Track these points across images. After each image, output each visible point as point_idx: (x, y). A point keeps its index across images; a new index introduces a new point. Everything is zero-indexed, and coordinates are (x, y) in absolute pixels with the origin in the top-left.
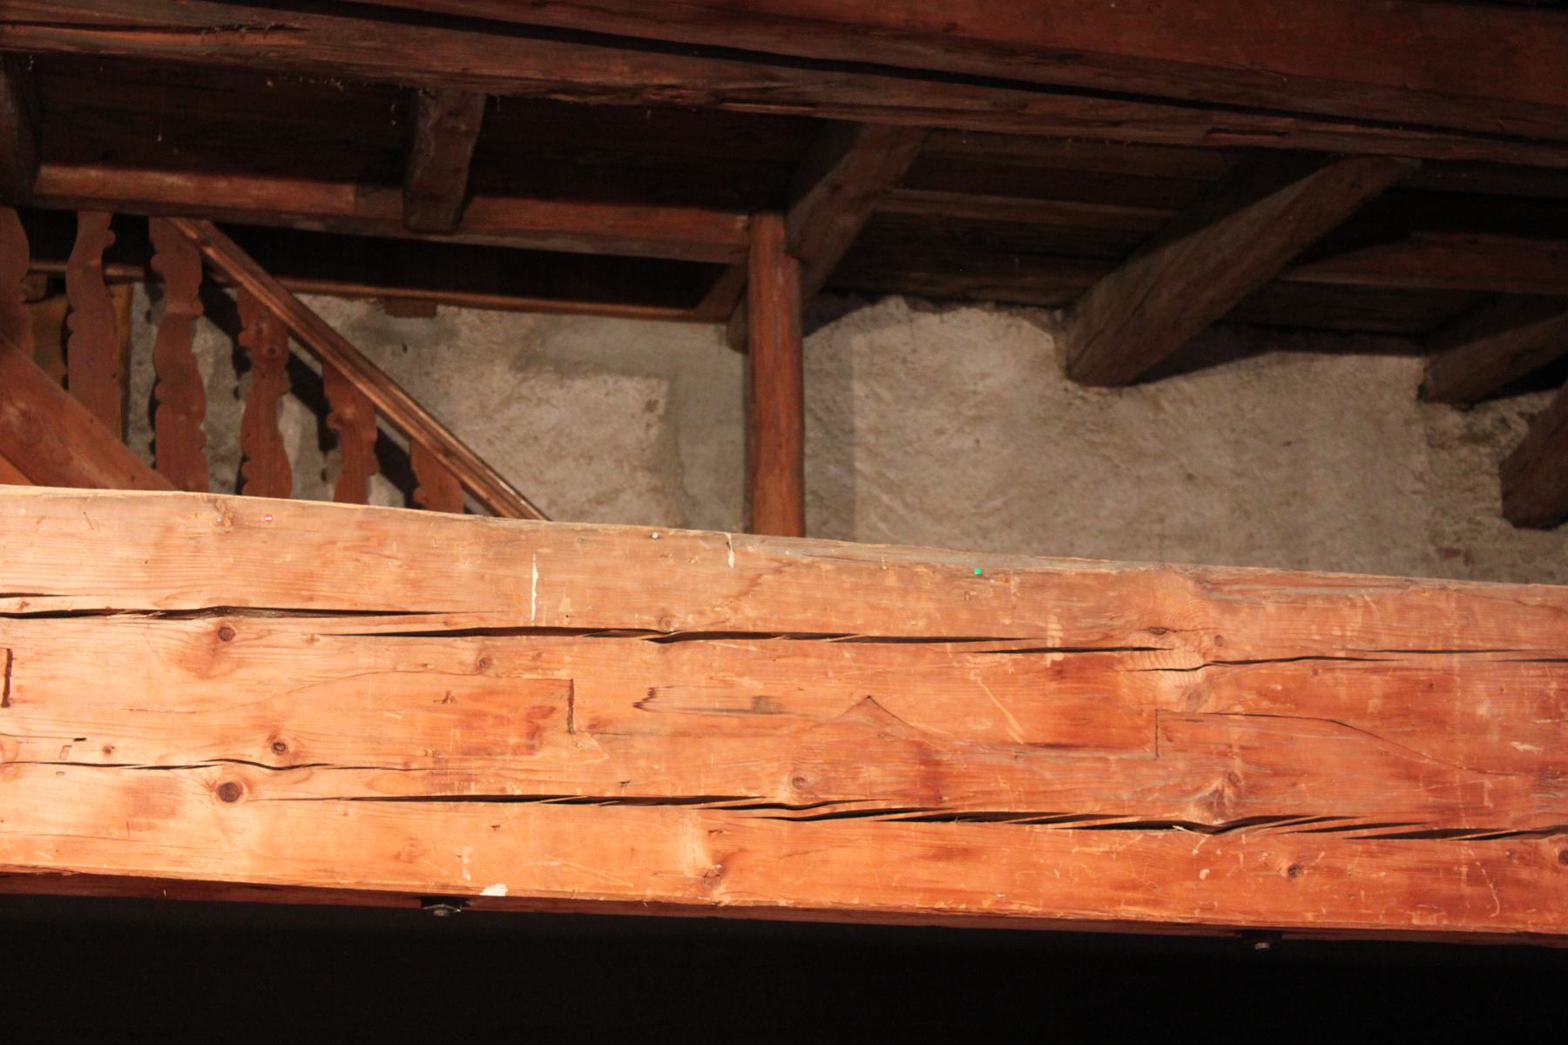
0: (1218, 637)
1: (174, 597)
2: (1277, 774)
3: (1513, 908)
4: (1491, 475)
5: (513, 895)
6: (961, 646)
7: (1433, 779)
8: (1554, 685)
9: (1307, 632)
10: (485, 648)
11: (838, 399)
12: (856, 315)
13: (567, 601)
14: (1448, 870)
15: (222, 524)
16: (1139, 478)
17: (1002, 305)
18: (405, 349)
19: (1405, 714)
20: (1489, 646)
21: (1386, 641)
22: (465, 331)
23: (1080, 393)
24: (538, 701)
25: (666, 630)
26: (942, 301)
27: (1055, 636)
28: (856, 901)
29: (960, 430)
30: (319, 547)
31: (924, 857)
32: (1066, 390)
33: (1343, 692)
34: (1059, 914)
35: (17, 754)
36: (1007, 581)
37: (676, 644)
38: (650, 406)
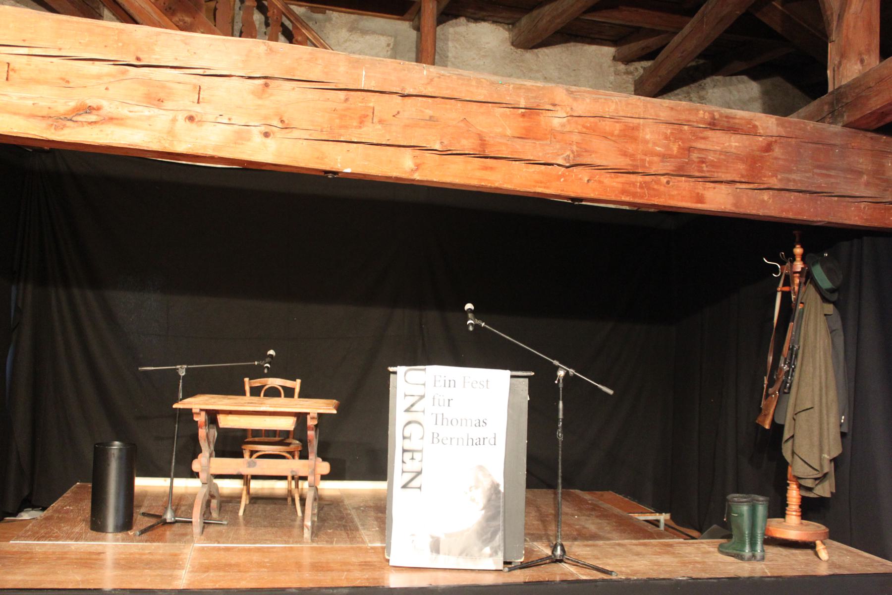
0: (572, 108)
1: (251, 72)
2: (586, 151)
3: (652, 196)
4: (632, 84)
5: (353, 172)
6: (494, 105)
7: (632, 156)
8: (669, 131)
9: (598, 109)
10: (347, 95)
11: (444, 47)
12: (451, 22)
13: (373, 82)
14: (633, 184)
15: (267, 50)
16: (531, 77)
17: (494, 22)
18: (316, 23)
19: (625, 136)
20: (651, 117)
21: (621, 114)
22: (334, 18)
23: (515, 50)
24: (363, 113)
25: (403, 93)
26: (477, 20)
27: (523, 104)
28: (457, 181)
29: (479, 59)
30: (297, 60)
31: (479, 169)
32: (511, 49)
33: (607, 128)
34: (518, 189)
35: (202, 118)
36: (509, 86)
37: (407, 98)
38: (388, 45)
